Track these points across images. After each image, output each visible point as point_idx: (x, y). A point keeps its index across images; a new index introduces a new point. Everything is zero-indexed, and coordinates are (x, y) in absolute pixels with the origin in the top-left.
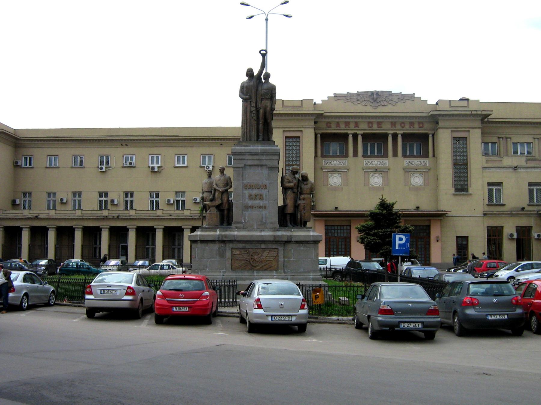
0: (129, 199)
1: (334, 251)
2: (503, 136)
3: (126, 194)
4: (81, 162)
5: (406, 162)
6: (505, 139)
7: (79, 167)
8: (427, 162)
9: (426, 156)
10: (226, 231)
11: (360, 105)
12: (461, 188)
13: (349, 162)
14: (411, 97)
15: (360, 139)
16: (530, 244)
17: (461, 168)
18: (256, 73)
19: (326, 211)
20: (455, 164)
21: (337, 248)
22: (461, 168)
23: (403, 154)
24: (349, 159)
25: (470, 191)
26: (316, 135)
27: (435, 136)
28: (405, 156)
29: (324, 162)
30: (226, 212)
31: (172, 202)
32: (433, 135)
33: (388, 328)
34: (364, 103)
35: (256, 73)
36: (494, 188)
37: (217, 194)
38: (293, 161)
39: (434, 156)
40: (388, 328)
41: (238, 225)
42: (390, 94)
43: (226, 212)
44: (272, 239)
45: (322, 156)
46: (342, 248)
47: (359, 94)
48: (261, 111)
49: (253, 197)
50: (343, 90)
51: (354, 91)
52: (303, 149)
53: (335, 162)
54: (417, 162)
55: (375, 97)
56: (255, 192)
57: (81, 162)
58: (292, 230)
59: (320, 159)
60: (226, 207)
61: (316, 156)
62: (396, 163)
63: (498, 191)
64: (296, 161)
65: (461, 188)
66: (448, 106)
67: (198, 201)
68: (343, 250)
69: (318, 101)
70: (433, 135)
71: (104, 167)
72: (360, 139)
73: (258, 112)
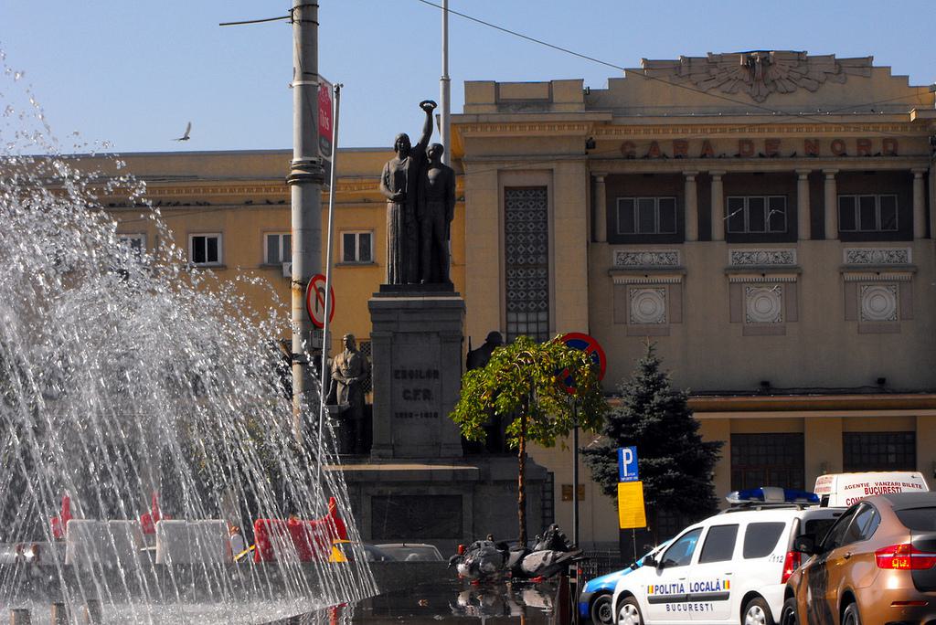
5: (850, 252)
9: (905, 234)
10: (360, 463)
11: (718, 93)
13: (689, 253)
14: (863, 65)
15: (717, 189)
18: (413, 144)
26: (592, 182)
27: (930, 179)
29: (617, 254)
30: (359, 425)
32: (926, 176)
34: (727, 86)
35: (413, 144)
37: (340, 388)
38: (527, 255)
39: (928, 235)
41: (383, 452)
42: (800, 57)
43: (359, 425)
44: (449, 479)
45: (613, 239)
47: (713, 62)
48: (427, 222)
49: (412, 395)
50: (671, 51)
52: (556, 221)
53: (648, 255)
54: (877, 252)
55: (759, 67)
56: (414, 384)
58: (490, 459)
59: (604, 248)
60: (359, 414)
61: (593, 238)
62: (821, 258)
64: (537, 254)
70: (926, 176)
72: (717, 189)
73: (420, 224)
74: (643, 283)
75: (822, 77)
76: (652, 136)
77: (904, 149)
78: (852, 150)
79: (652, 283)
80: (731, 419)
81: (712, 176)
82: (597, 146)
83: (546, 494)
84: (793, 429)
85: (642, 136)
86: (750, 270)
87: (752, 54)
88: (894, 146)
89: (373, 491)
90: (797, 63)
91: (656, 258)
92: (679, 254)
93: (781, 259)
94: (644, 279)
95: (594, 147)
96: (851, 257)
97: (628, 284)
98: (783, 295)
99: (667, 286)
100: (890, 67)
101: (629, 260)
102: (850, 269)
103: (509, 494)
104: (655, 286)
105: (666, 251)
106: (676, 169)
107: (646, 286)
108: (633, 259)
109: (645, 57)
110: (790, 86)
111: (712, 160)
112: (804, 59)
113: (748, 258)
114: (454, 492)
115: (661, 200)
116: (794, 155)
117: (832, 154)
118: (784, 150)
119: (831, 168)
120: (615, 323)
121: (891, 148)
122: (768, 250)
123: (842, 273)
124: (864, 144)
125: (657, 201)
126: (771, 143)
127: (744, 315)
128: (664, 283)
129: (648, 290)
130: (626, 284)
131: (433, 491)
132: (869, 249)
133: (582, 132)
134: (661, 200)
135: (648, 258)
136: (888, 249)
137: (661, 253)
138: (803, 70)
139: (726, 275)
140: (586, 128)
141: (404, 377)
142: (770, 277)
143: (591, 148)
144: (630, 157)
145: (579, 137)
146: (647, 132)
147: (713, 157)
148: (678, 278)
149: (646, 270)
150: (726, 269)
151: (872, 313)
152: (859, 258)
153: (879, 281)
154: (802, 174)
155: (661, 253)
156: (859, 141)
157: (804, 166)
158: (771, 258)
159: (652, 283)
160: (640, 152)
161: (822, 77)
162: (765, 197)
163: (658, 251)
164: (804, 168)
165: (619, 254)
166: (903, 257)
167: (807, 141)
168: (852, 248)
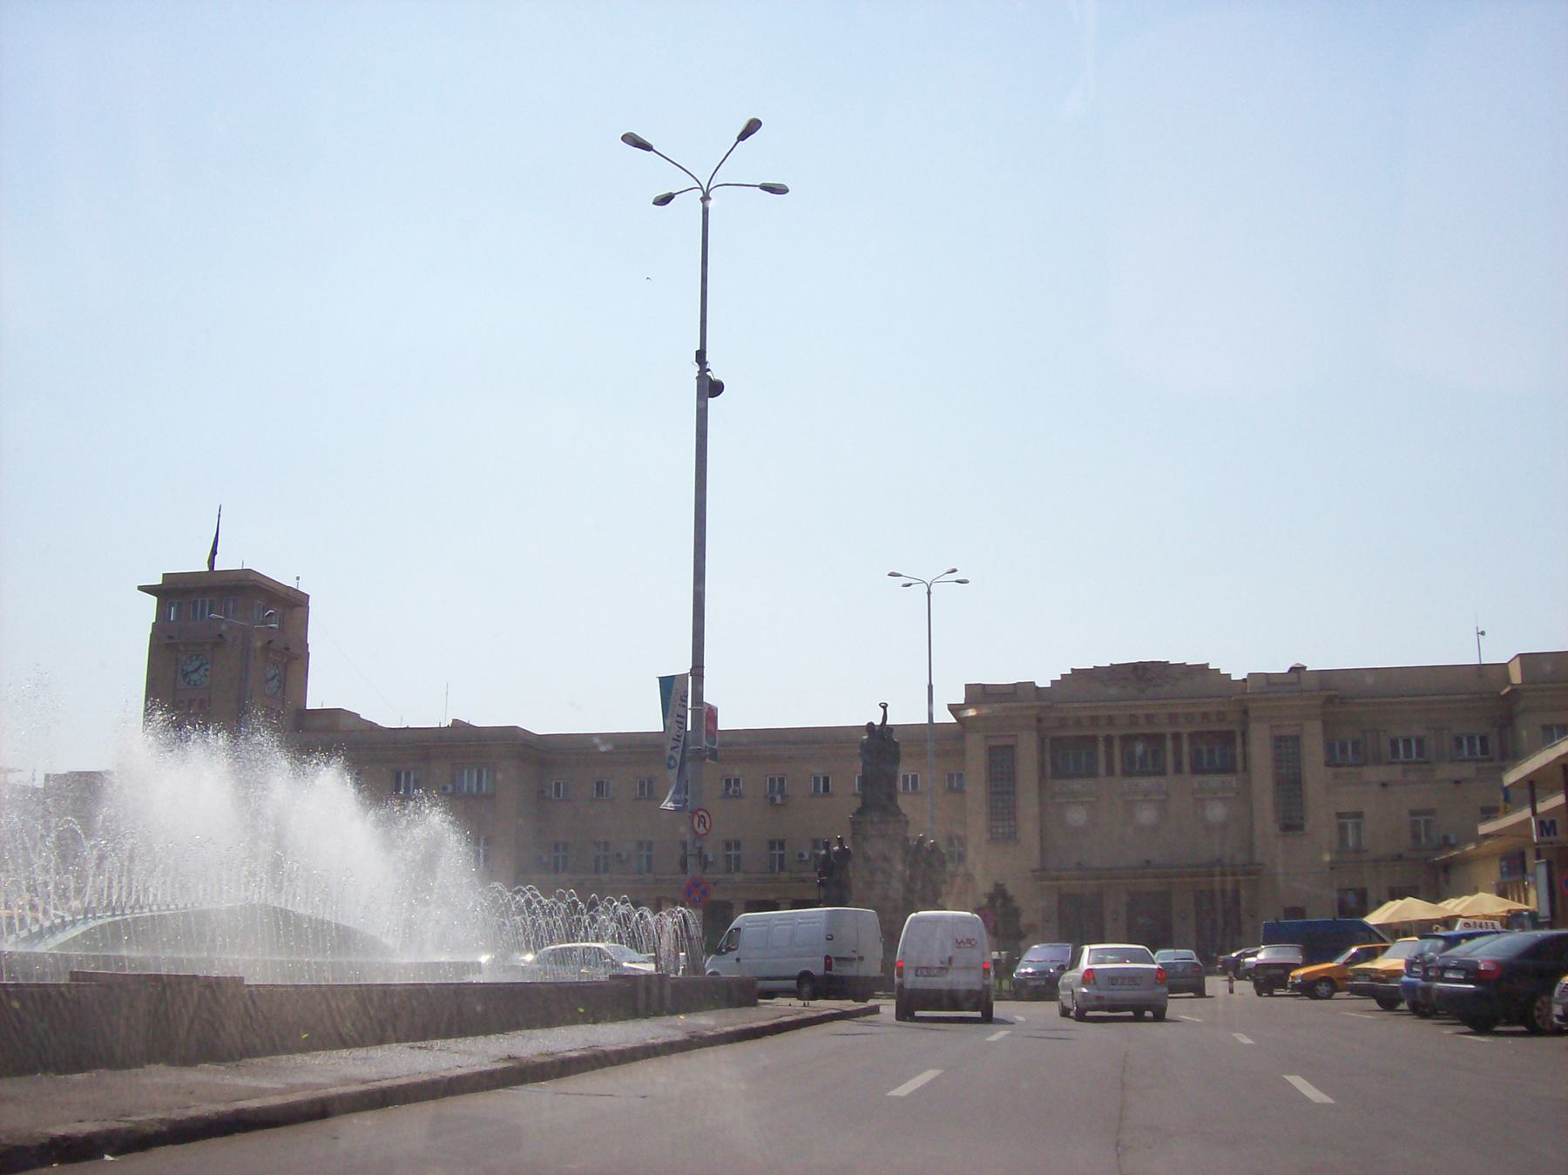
0: (732, 852)
3: (728, 845)
4: (826, 788)
7: (1416, 763)
8: (1233, 780)
12: (1291, 825)
15: (1117, 744)
17: (1290, 785)
22: (1290, 785)
25: (1307, 828)
26: (1042, 741)
31: (807, 857)
33: (917, 1013)
36: (1422, 819)
39: (1245, 769)
40: (917, 1013)
51: (1105, 663)
57: (826, 788)
63: (1358, 827)
65: (1291, 825)
67: (807, 857)
69: (1043, 683)
70: (1244, 734)
71: (779, 799)
72: (1117, 744)
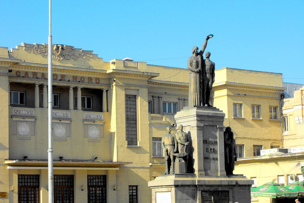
1: (99, 196)
2: (157, 95)
6: (183, 101)
12: (132, 140)
13: (71, 113)
15: (79, 93)
16: (54, 188)
19: (82, 161)
20: (127, 119)
21: (27, 198)
22: (131, 121)
23: (82, 107)
24: (36, 109)
28: (84, 109)
32: (107, 91)
36: (157, 142)
44: (227, 184)
46: (31, 197)
65: (132, 140)
66: (123, 66)
68: (98, 195)
70: (107, 91)
72: (79, 93)
74: (22, 121)
75: (78, 56)
76: (26, 70)
77: (102, 82)
78: (31, 75)
79: (25, 121)
80: (88, 170)
81: (44, 85)
82: (12, 71)
83: (61, 193)
84: (103, 174)
85: (23, 70)
86: (90, 120)
87: (58, 45)
88: (56, 76)
89: (202, 189)
90: (71, 50)
91: (26, 113)
92: (34, 111)
93: (65, 116)
94: (23, 120)
95: (12, 72)
96: (86, 116)
97: (18, 121)
98: (66, 128)
99: (66, 124)
100: (98, 55)
101: (18, 113)
102: (86, 120)
103: (242, 190)
104: (26, 122)
105: (30, 110)
106: (33, 82)
107: (23, 122)
108: (19, 112)
109: (25, 42)
110: (69, 57)
111: (28, 78)
112: (73, 49)
113: (55, 114)
114: (227, 189)
115: (20, 93)
116: (69, 81)
117: (16, 76)
118: (67, 79)
119: (81, 86)
120: (13, 135)
121: (98, 81)
122: (61, 112)
123: (83, 122)
124: (90, 79)
125: (19, 93)
126: (63, 76)
127: (54, 134)
128: (29, 121)
129: (23, 124)
130: (17, 121)
131: (220, 189)
132: (91, 114)
133: (8, 66)
134: (20, 93)
135: (24, 112)
136: (97, 114)
137: (28, 111)
138: (73, 52)
139: (83, 122)
140: (10, 64)
141: (207, 158)
142: (62, 121)
143: (10, 72)
144: (19, 76)
145: (7, 68)
146: (94, 74)
147: (65, 80)
148: (33, 120)
149: (24, 117)
150: (83, 120)
151: (91, 134)
152: (88, 117)
153: (94, 125)
154: (71, 87)
155: (28, 111)
156: (89, 78)
157: (72, 85)
158: (62, 115)
159: (25, 121)
160: (22, 75)
161: (78, 56)
162: (18, 92)
163: (27, 110)
164: (72, 85)
165: (14, 110)
166: (32, 113)
167: (73, 76)
168: (86, 113)
